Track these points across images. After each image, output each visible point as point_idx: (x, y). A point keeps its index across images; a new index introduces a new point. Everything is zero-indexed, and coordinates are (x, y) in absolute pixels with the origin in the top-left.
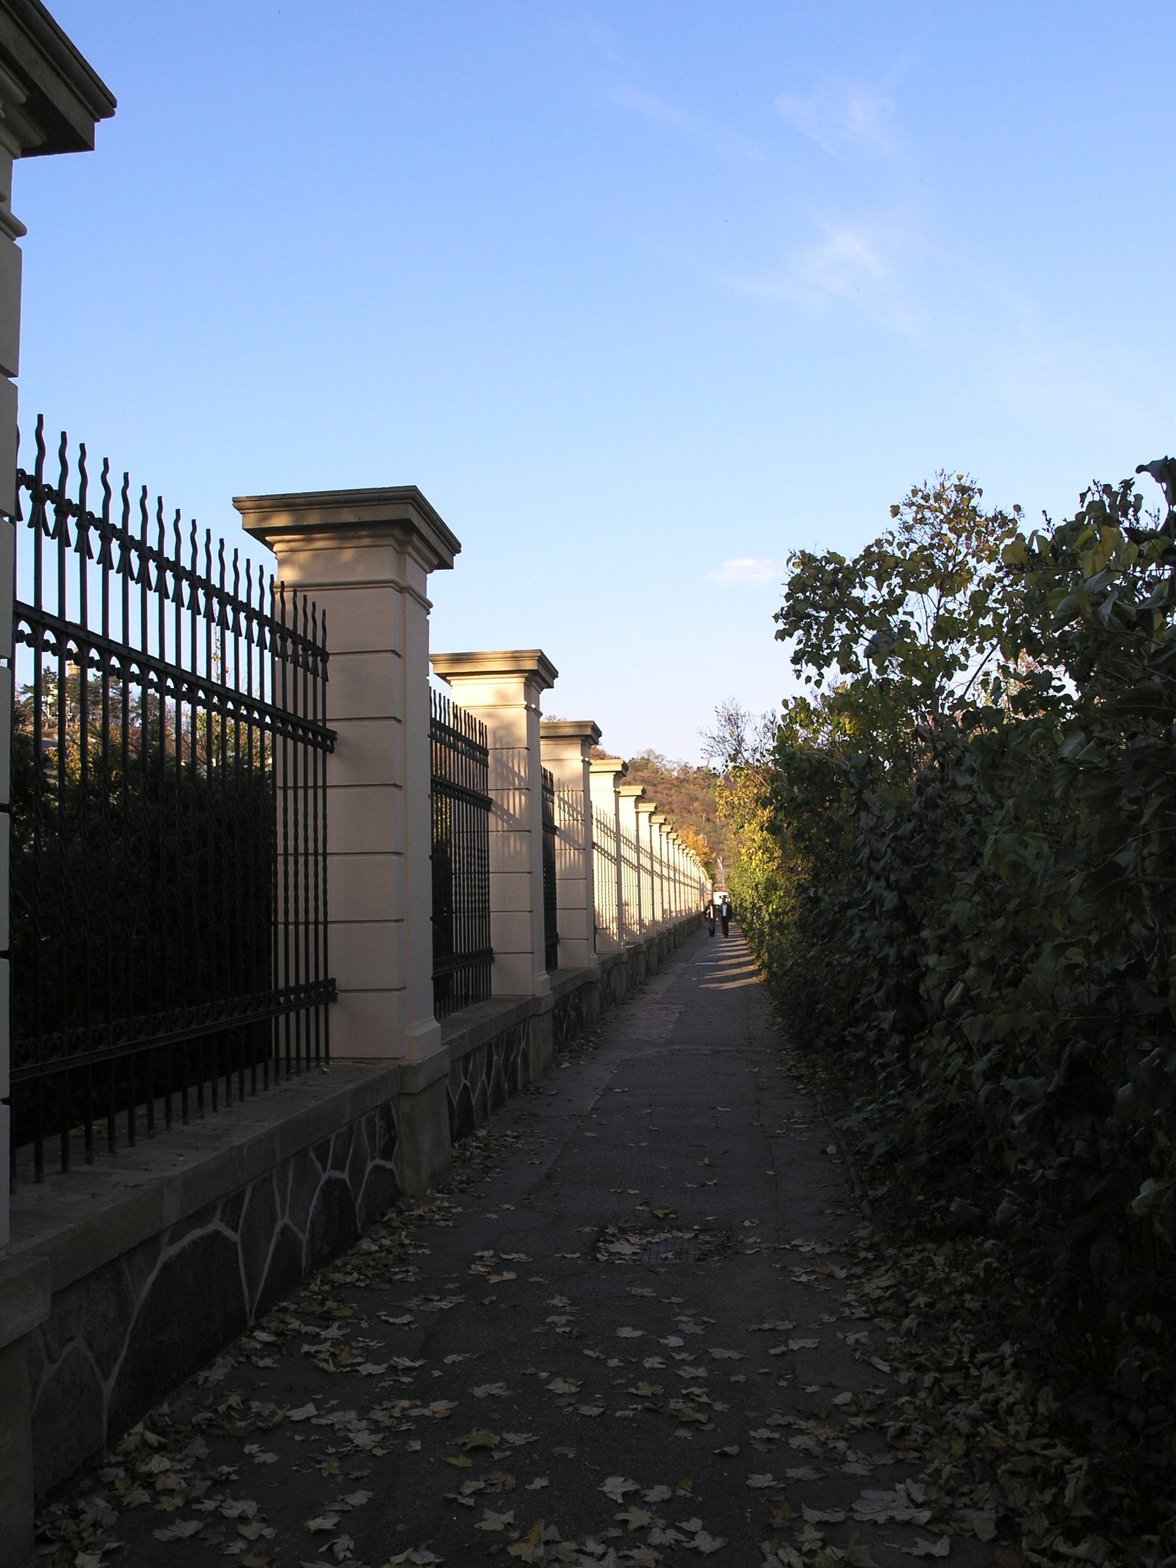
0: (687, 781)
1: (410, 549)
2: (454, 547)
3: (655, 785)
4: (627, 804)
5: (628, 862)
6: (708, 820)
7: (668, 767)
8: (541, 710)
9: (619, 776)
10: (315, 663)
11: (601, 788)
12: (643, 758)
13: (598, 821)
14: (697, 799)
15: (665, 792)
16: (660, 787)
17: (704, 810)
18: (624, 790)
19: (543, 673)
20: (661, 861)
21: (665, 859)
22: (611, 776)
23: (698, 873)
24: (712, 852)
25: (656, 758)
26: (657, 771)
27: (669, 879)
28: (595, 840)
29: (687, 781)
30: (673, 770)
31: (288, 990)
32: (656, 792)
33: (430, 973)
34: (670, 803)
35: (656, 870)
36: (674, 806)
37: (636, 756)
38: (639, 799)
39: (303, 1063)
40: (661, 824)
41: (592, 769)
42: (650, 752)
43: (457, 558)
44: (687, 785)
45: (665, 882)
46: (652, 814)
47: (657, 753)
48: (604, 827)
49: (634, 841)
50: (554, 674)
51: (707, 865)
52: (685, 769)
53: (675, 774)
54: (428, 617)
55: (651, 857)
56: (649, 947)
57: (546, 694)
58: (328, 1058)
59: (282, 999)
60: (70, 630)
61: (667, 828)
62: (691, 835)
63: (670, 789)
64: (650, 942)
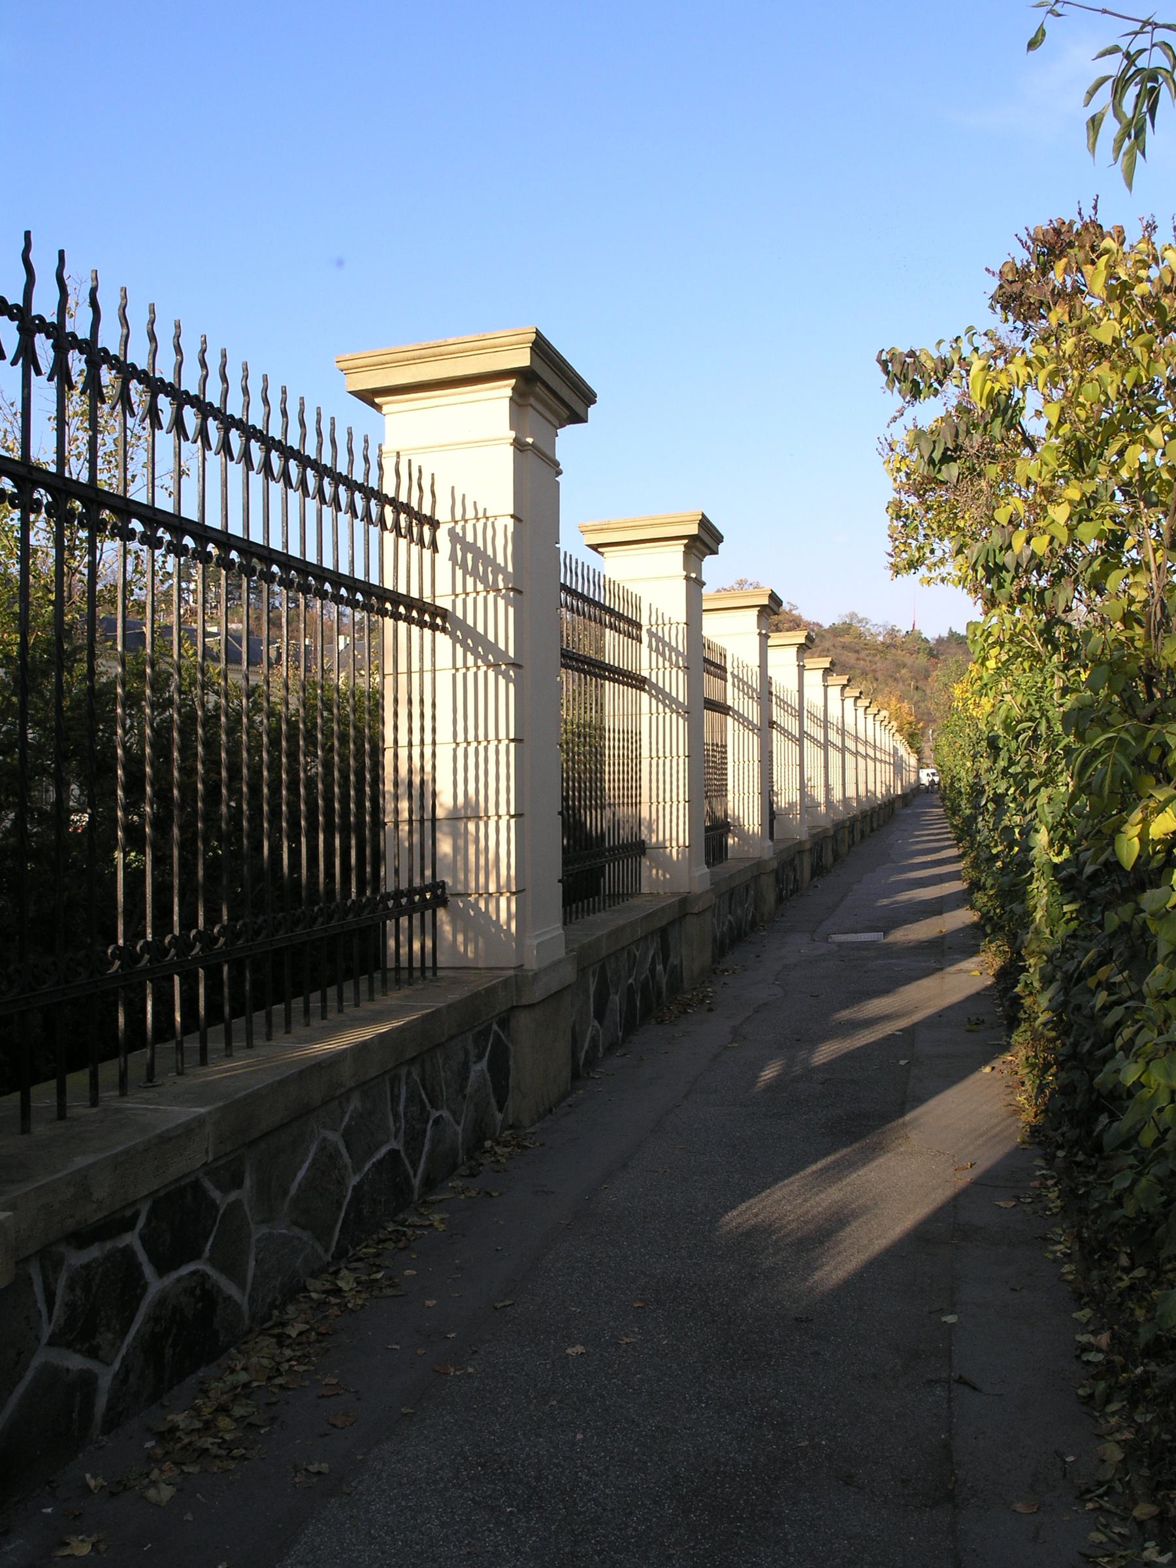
0: (894, 646)
1: (532, 401)
2: (589, 397)
3: (857, 652)
4: (814, 678)
5: (813, 739)
6: (917, 688)
7: (873, 631)
8: (704, 579)
9: (802, 649)
10: (485, 571)
11: (783, 664)
12: (845, 623)
13: (777, 697)
14: (904, 666)
15: (868, 659)
16: (863, 654)
17: (912, 678)
18: (809, 663)
19: (707, 539)
20: (875, 746)
21: (861, 735)
22: (795, 649)
23: (890, 740)
24: (918, 722)
25: (860, 621)
26: (860, 636)
27: (866, 756)
28: (774, 719)
29: (894, 646)
30: (878, 635)
31: (398, 894)
32: (858, 659)
33: (558, 873)
34: (874, 671)
35: (835, 741)
36: (878, 675)
37: (837, 621)
38: (827, 672)
39: (404, 975)
40: (857, 698)
41: (770, 642)
42: (853, 615)
43: (592, 410)
44: (894, 651)
45: (861, 761)
46: (844, 687)
47: (861, 616)
48: (783, 704)
49: (756, 683)
50: (719, 538)
51: (913, 739)
52: (892, 633)
53: (881, 638)
54: (513, 434)
55: (843, 732)
56: (836, 832)
57: (709, 560)
58: (435, 967)
59: (391, 903)
60: (326, 575)
61: (864, 702)
62: (894, 701)
63: (875, 655)
64: (839, 826)
